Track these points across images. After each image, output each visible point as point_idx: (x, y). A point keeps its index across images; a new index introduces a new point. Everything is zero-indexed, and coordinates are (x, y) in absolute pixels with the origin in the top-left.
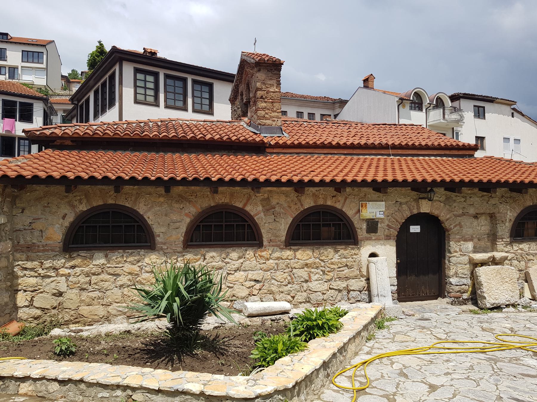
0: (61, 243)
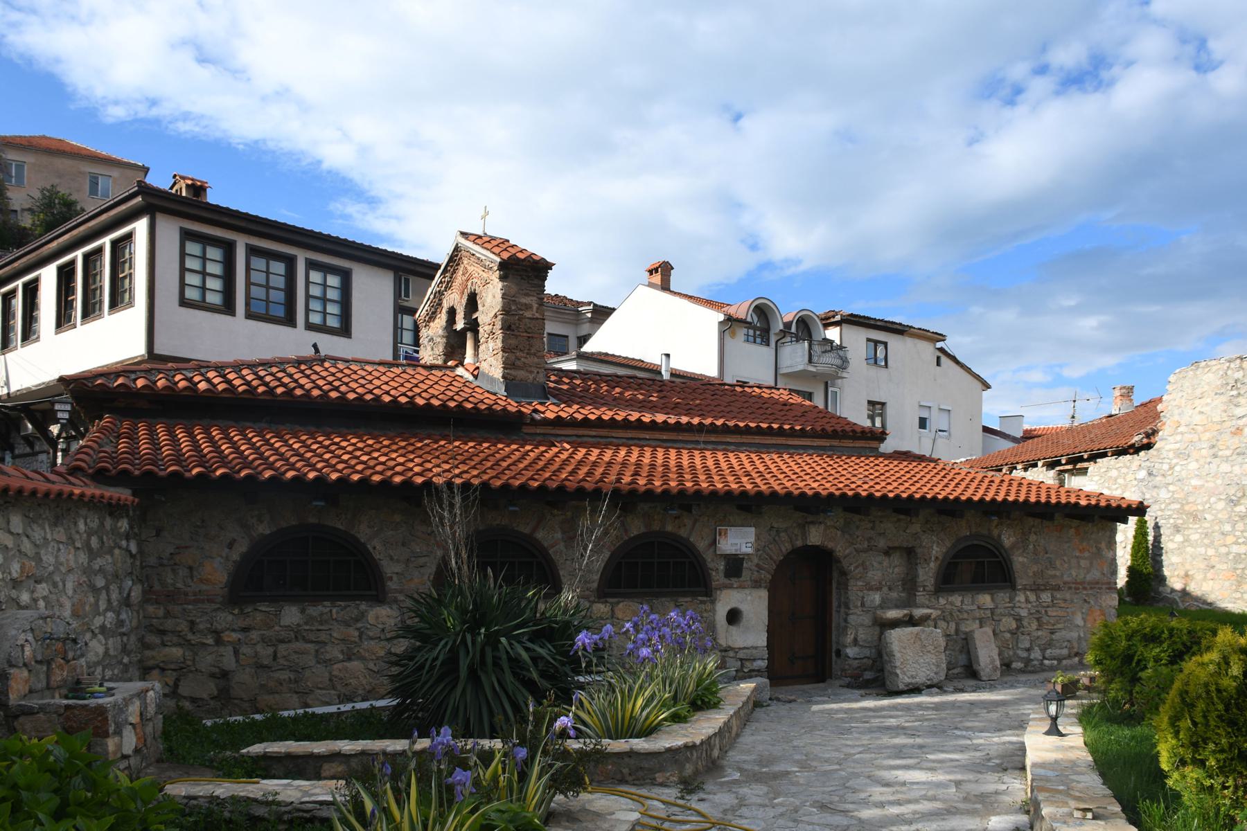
0: (226, 589)
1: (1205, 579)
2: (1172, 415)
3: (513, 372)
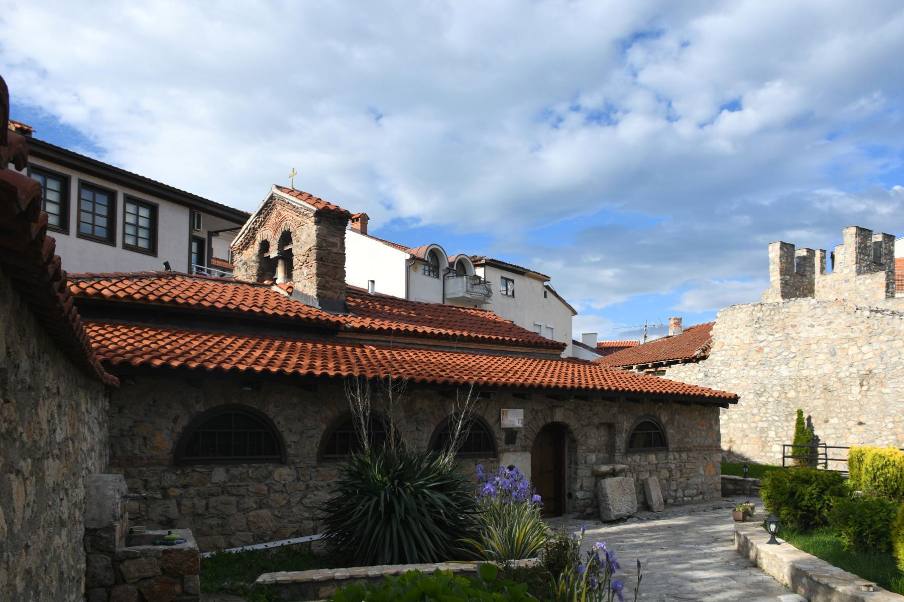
0: (172, 455)
1: (742, 444)
2: (719, 338)
3: (323, 292)
